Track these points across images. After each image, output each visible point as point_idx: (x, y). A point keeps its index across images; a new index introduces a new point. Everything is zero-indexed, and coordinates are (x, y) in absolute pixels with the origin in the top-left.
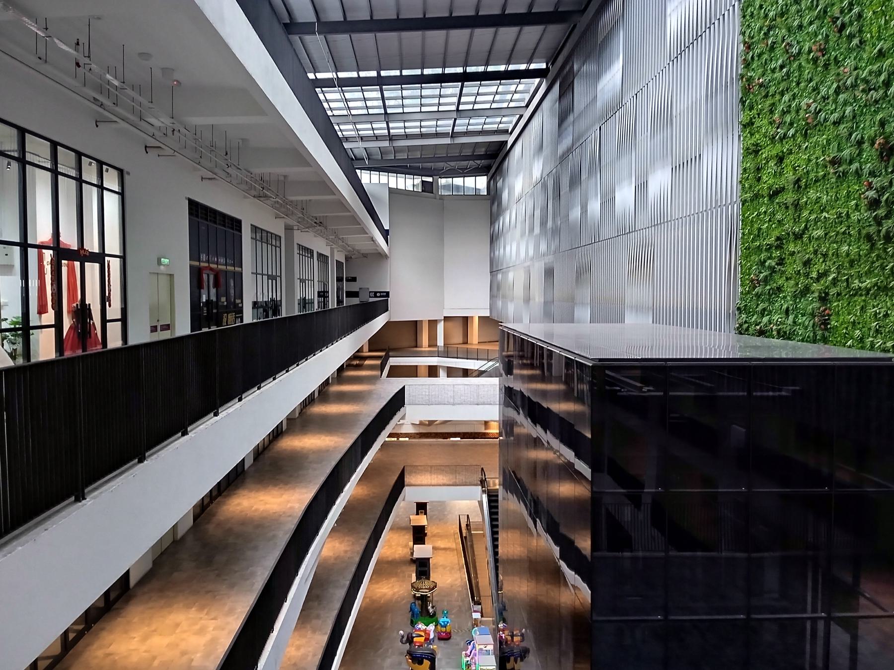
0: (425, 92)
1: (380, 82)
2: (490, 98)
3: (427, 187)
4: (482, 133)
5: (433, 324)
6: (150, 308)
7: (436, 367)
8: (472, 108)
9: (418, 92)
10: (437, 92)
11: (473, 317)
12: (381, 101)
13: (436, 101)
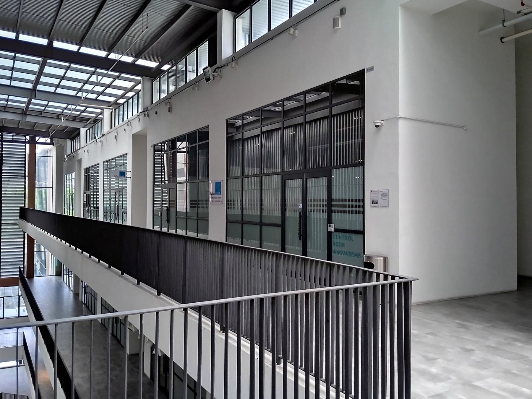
0: (18, 65)
6: (56, 319)
8: (53, 91)
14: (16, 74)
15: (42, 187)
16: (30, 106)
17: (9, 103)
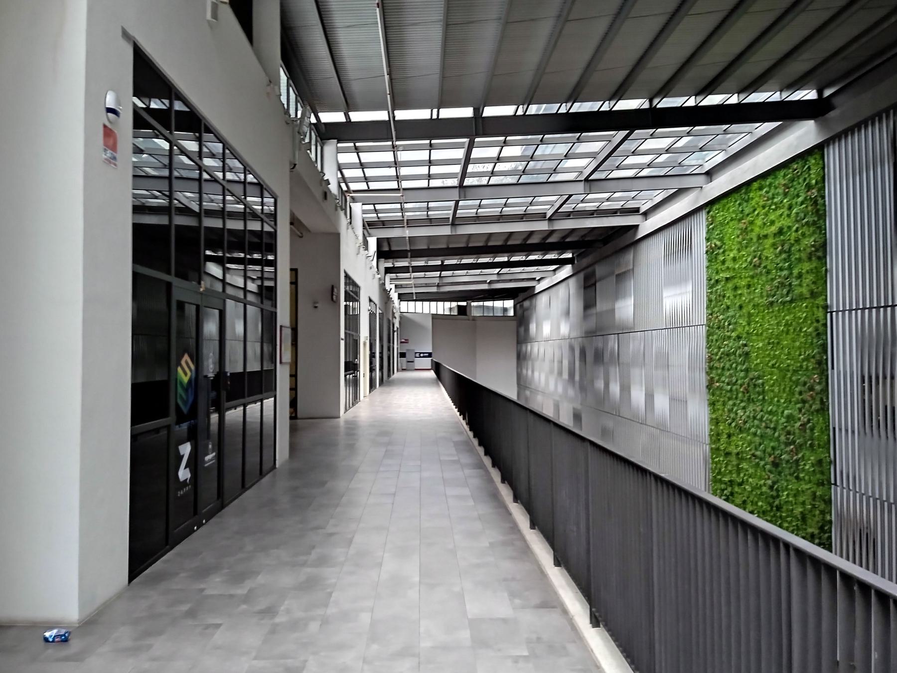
0: (437, 155)
2: (489, 167)
3: (462, 311)
4: (501, 218)
9: (423, 155)
10: (423, 155)
12: (222, 173)
13: (424, 170)
14: (435, 170)
15: (644, 331)
16: (458, 211)
17: (429, 213)
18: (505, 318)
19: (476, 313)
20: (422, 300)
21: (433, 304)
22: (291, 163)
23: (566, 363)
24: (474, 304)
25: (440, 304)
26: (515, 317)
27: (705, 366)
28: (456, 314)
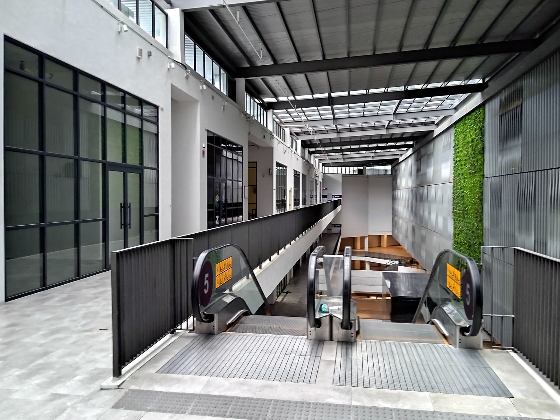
1: (331, 101)
3: (360, 172)
5: (363, 239)
7: (364, 262)
11: (383, 235)
18: (386, 175)
19: (368, 173)
20: (341, 166)
21: (344, 168)
22: (248, 132)
23: (410, 201)
24: (367, 168)
25: (348, 168)
26: (391, 175)
27: (452, 200)
28: (357, 173)
